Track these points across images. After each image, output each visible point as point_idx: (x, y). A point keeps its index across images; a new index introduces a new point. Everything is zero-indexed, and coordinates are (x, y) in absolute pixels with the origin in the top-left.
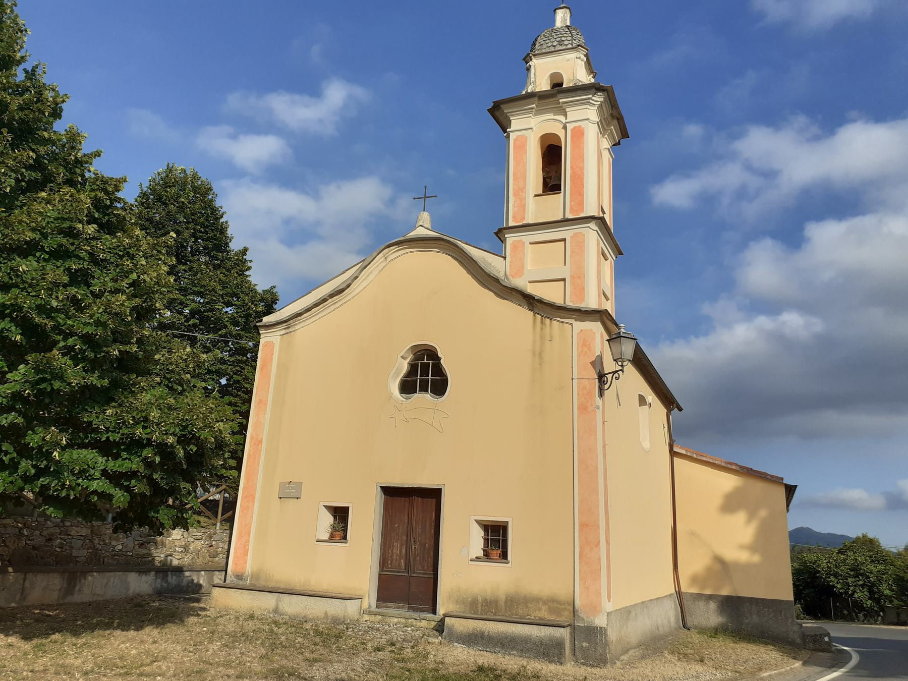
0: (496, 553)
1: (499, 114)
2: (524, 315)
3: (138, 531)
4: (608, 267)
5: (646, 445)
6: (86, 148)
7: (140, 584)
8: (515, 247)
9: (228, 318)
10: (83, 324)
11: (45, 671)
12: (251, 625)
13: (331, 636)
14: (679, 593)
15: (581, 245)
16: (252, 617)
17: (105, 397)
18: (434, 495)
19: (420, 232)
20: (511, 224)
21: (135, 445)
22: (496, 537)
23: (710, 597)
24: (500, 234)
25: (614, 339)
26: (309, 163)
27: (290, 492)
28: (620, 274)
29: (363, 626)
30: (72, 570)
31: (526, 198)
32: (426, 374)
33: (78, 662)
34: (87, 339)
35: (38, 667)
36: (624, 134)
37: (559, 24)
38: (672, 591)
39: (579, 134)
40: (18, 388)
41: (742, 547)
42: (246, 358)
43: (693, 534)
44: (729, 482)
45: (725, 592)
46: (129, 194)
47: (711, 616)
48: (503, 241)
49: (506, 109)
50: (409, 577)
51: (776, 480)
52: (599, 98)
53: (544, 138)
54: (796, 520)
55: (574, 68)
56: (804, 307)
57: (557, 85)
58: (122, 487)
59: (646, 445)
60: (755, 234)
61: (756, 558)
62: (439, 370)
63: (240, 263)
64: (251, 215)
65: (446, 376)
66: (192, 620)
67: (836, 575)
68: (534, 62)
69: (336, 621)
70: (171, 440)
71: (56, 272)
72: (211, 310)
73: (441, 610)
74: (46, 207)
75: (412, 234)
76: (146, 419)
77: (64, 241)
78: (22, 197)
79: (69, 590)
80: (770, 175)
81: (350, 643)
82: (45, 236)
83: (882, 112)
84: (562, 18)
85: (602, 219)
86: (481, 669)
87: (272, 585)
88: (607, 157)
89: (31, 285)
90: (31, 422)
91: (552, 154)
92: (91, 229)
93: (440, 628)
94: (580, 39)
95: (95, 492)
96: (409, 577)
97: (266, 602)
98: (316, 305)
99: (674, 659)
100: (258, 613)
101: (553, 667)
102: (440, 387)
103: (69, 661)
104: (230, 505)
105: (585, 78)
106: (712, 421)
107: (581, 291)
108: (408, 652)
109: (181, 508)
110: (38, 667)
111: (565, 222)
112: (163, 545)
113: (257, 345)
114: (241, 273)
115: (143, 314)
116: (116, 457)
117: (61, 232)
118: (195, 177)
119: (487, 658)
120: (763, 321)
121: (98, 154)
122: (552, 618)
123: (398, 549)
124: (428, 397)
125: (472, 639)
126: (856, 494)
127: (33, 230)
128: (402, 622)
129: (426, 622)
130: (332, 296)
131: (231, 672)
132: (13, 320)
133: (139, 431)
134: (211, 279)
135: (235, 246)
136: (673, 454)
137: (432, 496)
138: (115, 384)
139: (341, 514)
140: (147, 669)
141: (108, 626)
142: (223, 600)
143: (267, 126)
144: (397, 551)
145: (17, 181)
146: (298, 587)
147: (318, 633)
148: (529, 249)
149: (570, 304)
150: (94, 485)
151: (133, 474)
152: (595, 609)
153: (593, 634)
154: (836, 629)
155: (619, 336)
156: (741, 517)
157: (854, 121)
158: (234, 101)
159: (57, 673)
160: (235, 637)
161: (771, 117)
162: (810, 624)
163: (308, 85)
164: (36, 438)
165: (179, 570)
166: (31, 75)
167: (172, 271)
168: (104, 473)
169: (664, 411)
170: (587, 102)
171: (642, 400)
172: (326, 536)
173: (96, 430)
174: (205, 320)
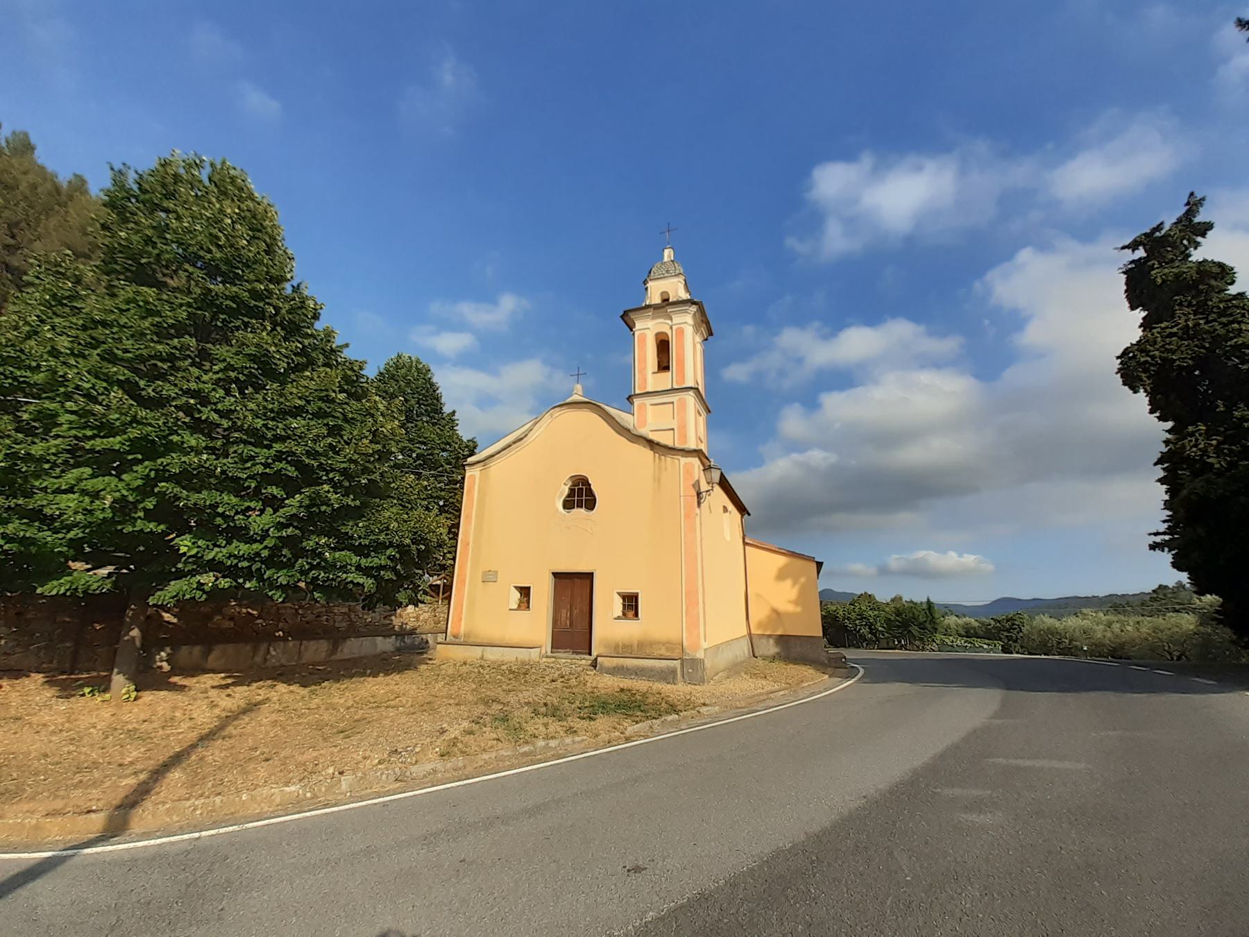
0: (631, 614)
1: (627, 319)
2: (647, 453)
3: (380, 608)
4: (702, 420)
5: (728, 538)
6: (337, 342)
7: (385, 644)
8: (640, 406)
9: (443, 460)
10: (339, 462)
11: (318, 707)
12: (465, 669)
13: (521, 673)
14: (750, 634)
15: (683, 405)
16: (465, 664)
17: (357, 514)
18: (590, 576)
19: (576, 398)
20: (637, 392)
21: (380, 547)
22: (631, 603)
23: (770, 636)
24: (630, 398)
25: (707, 469)
26: (490, 352)
27: (489, 577)
28: (710, 426)
29: (543, 666)
30: (336, 637)
31: (647, 375)
32: (581, 495)
33: (342, 701)
34: (344, 472)
35: (313, 706)
36: (711, 334)
37: (666, 259)
38: (745, 632)
39: (681, 332)
40: (294, 511)
41: (790, 602)
42: (457, 486)
43: (758, 595)
44: (781, 560)
45: (779, 633)
46: (371, 372)
47: (771, 648)
48: (632, 403)
49: (632, 316)
50: (573, 631)
51: (811, 559)
52: (694, 309)
53: (657, 335)
54: (822, 585)
55: (676, 288)
56: (823, 446)
57: (666, 300)
58: (372, 576)
59: (728, 538)
60: (789, 399)
61: (799, 609)
62: (590, 493)
63: (451, 420)
64: (456, 388)
65: (594, 496)
66: (423, 667)
67: (848, 619)
68: (650, 284)
69: (523, 663)
70: (408, 541)
71: (318, 429)
72: (432, 454)
73: (594, 653)
74: (309, 381)
75: (569, 400)
76: (388, 529)
77: (323, 405)
78: (292, 376)
79: (334, 651)
80: (800, 361)
81: (534, 677)
82: (308, 402)
83: (872, 318)
84: (668, 254)
85: (697, 389)
86: (622, 690)
87: (478, 641)
88: (699, 347)
89: (300, 437)
90: (306, 534)
91: (663, 346)
92: (342, 396)
93: (594, 664)
94: (680, 269)
95: (352, 582)
96: (573, 631)
97: (474, 653)
98: (504, 449)
99: (747, 677)
100: (469, 661)
101: (669, 686)
102: (590, 503)
103: (335, 700)
104: (448, 588)
105: (684, 296)
106: (763, 521)
107: (684, 437)
108: (573, 682)
109: (416, 589)
110: (313, 706)
111: (673, 390)
112: (401, 616)
113: (463, 478)
114: (452, 428)
115: (384, 456)
116: (367, 556)
117: (320, 399)
118: (418, 362)
119: (626, 683)
120: (795, 456)
121: (347, 345)
122: (668, 654)
123: (564, 613)
124: (583, 510)
125: (615, 671)
126: (858, 567)
127: (300, 398)
128: (568, 661)
129: (585, 661)
130: (514, 442)
131: (452, 701)
132: (288, 462)
133: (382, 537)
134: (430, 432)
135: (447, 410)
136: (745, 544)
137: (528, 588)
138: (364, 505)
139: (525, 592)
140: (393, 703)
141: (363, 675)
142: (442, 652)
143: (458, 326)
144: (564, 615)
145: (288, 364)
146: (498, 642)
147: (511, 672)
148: (649, 408)
149: (678, 445)
150: (351, 577)
151: (381, 567)
152: (697, 647)
153: (696, 663)
154: (850, 653)
155: (710, 467)
156: (789, 582)
157: (849, 325)
158: (435, 308)
159: (327, 709)
160: (453, 679)
161: (799, 320)
162: (832, 651)
163: (487, 297)
164: (311, 543)
165: (412, 632)
166: (296, 289)
167: (402, 426)
168: (359, 568)
169: (739, 516)
170: (686, 312)
171: (725, 510)
172: (515, 606)
173: (352, 537)
174: (427, 461)
